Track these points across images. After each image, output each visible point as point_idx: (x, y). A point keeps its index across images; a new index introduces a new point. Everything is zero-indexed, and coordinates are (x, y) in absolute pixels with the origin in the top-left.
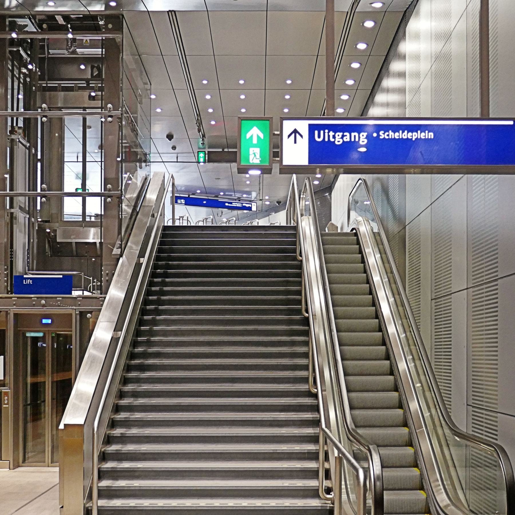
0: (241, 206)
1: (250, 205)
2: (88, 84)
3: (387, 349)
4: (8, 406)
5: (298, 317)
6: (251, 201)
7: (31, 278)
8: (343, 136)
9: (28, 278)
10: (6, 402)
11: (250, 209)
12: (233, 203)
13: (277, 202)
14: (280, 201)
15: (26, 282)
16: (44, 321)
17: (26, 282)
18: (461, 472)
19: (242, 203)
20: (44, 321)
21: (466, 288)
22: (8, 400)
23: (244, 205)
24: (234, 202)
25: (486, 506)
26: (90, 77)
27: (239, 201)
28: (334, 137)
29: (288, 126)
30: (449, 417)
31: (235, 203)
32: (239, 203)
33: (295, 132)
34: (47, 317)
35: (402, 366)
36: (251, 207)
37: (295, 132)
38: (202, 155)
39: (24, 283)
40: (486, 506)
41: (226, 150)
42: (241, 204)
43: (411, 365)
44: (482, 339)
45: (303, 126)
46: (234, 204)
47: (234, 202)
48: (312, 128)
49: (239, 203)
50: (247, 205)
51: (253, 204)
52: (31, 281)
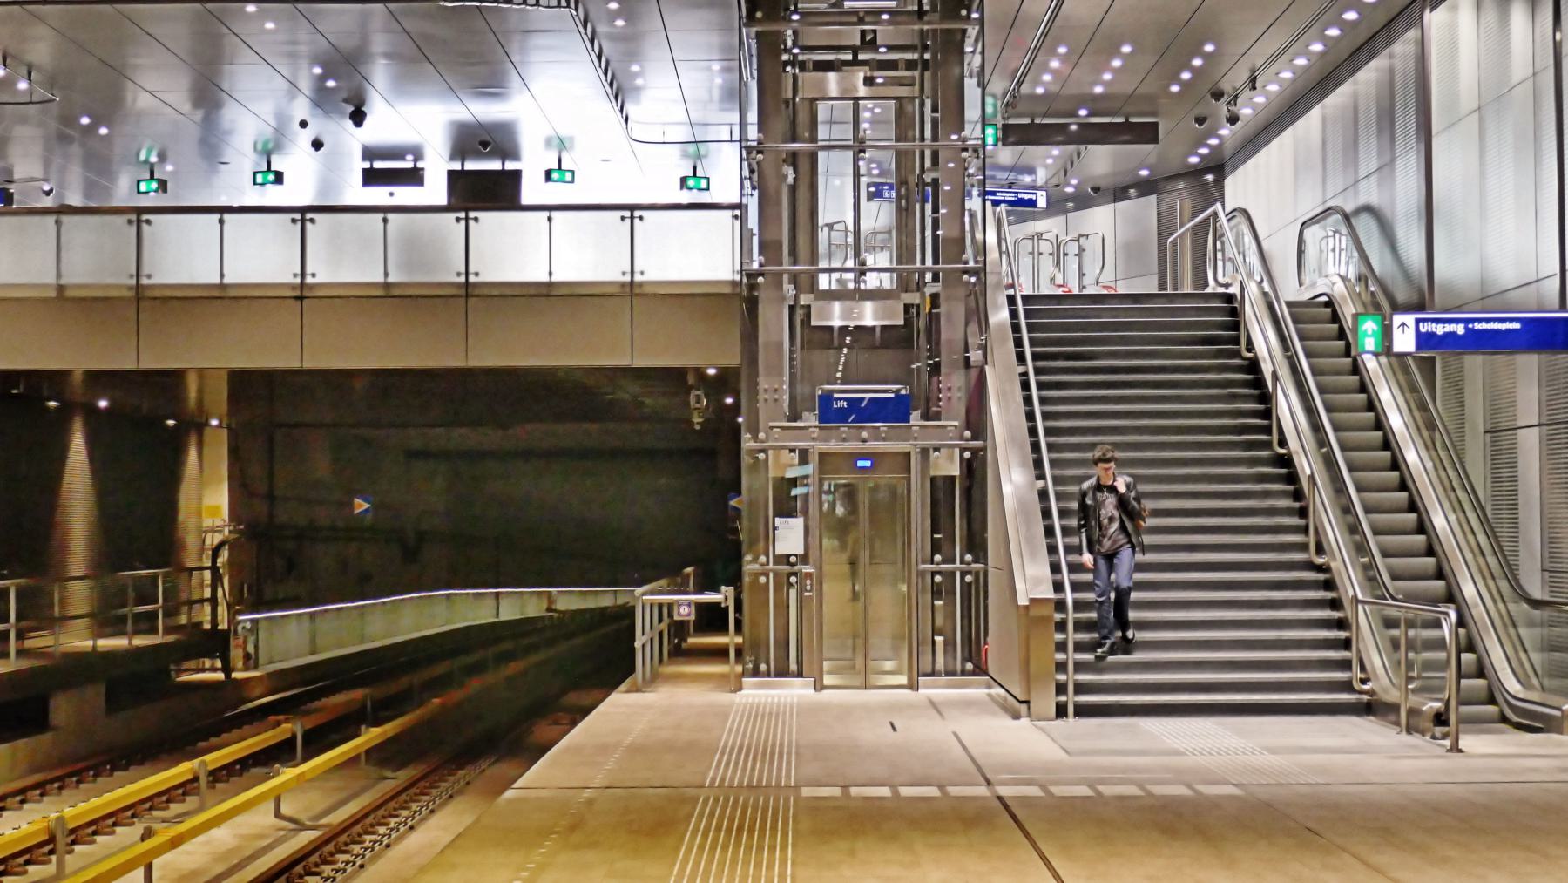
0: (1013, 199)
1: (1034, 197)
2: (855, 55)
3: (1411, 495)
4: (811, 594)
5: (1265, 453)
6: (1034, 188)
7: (845, 399)
8: (1444, 327)
9: (840, 399)
10: (808, 588)
11: (1033, 203)
12: (997, 194)
13: (1092, 189)
14: (1097, 186)
15: (837, 404)
16: (860, 463)
17: (837, 404)
18: (1536, 657)
19: (1017, 193)
20: (860, 463)
21: (1536, 422)
22: (811, 585)
23: (1020, 196)
24: (999, 192)
25: (1560, 525)
26: (858, 42)
27: (1010, 187)
28: (1436, 328)
29: (1398, 319)
30: (1517, 581)
31: (1002, 192)
32: (1011, 192)
33: (1403, 324)
34: (864, 456)
35: (1438, 521)
36: (1036, 201)
37: (1403, 324)
38: (990, 131)
39: (835, 406)
40: (1560, 525)
41: (1037, 121)
42: (1013, 195)
43: (1452, 518)
44: (1560, 473)
45: (1410, 319)
46: (1000, 194)
47: (999, 192)
48: (1418, 321)
49: (1011, 192)
50: (1026, 197)
51: (1039, 193)
52: (845, 403)
